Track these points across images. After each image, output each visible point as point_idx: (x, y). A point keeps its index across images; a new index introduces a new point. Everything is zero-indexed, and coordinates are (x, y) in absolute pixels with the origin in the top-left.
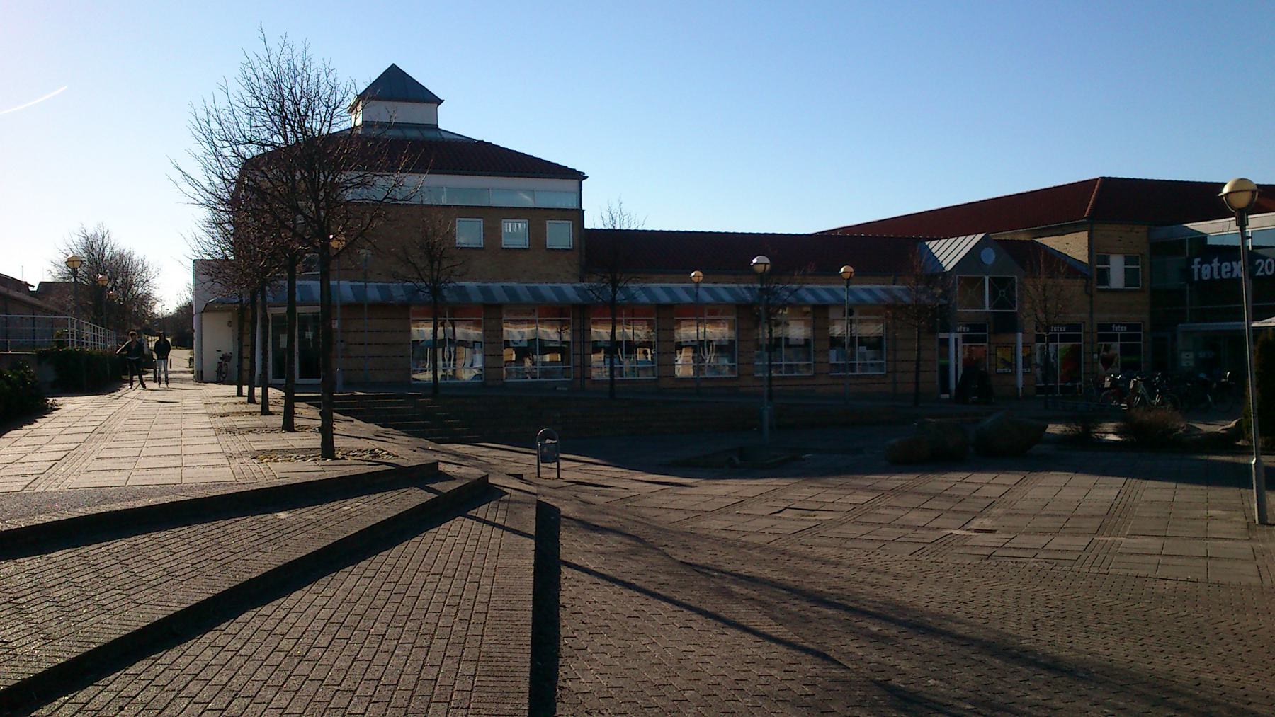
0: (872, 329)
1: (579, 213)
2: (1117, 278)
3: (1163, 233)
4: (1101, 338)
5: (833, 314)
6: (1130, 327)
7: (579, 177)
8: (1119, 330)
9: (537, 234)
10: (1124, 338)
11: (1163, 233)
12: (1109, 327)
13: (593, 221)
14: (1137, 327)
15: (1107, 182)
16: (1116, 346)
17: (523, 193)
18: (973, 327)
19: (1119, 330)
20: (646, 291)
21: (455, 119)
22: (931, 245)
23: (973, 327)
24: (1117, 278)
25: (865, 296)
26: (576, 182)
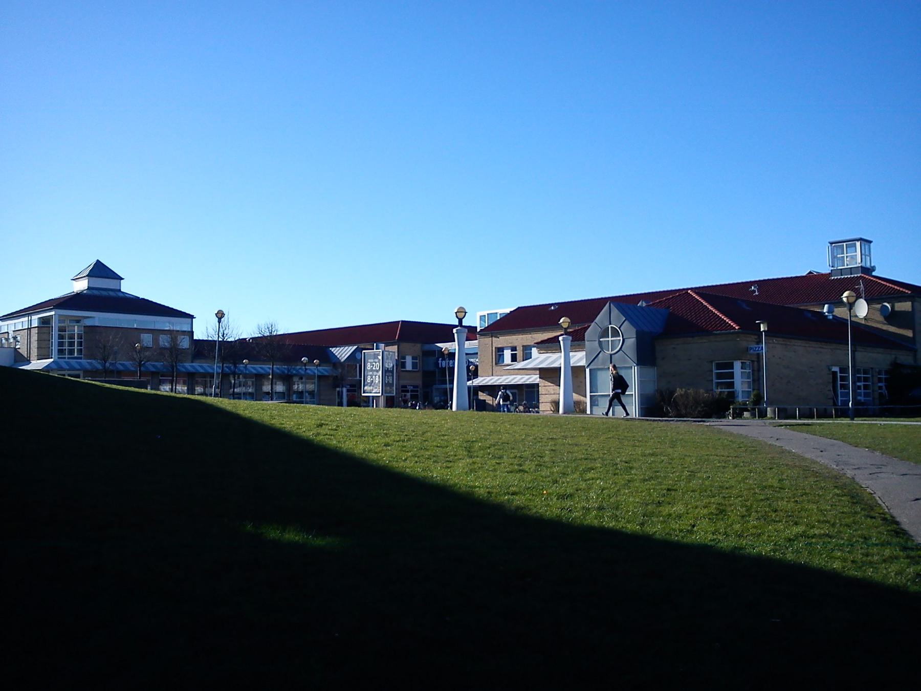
0: (310, 387)
1: (192, 332)
2: (409, 367)
3: (427, 347)
4: (403, 391)
5: (295, 379)
6: (414, 387)
7: (192, 317)
8: (410, 388)
9: (155, 340)
10: (412, 391)
11: (427, 347)
12: (405, 387)
13: (195, 337)
14: (417, 387)
15: (404, 323)
16: (409, 395)
17: (165, 323)
18: (351, 386)
19: (410, 388)
20: (184, 367)
21: (130, 287)
22: (333, 350)
23: (351, 386)
24: (409, 367)
25: (189, 368)
26: (189, 320)
